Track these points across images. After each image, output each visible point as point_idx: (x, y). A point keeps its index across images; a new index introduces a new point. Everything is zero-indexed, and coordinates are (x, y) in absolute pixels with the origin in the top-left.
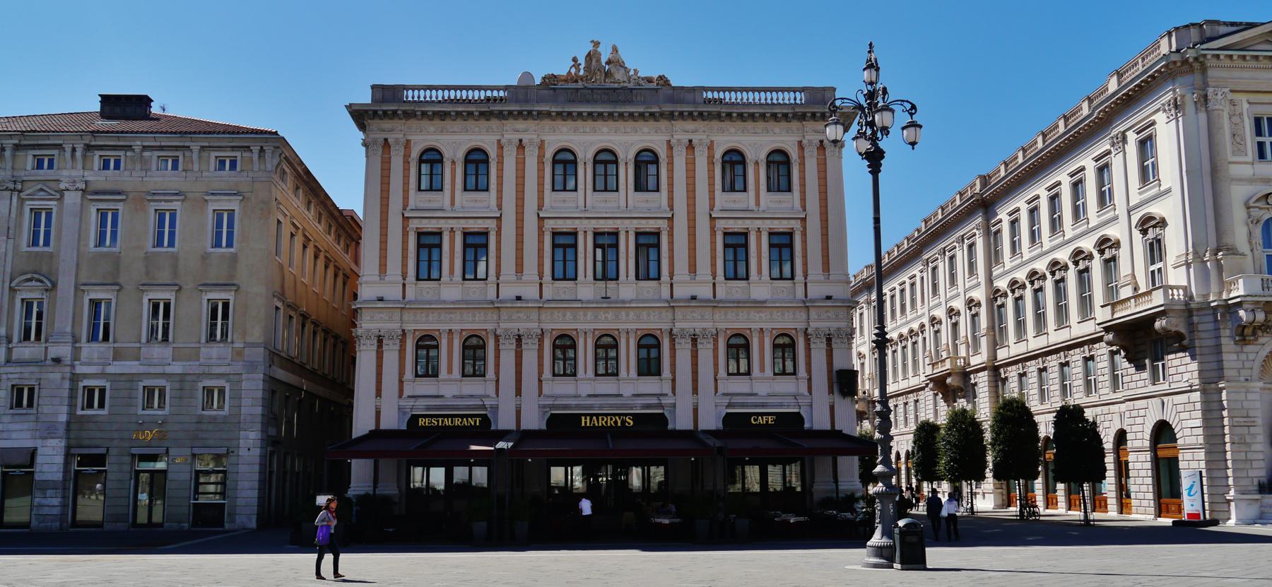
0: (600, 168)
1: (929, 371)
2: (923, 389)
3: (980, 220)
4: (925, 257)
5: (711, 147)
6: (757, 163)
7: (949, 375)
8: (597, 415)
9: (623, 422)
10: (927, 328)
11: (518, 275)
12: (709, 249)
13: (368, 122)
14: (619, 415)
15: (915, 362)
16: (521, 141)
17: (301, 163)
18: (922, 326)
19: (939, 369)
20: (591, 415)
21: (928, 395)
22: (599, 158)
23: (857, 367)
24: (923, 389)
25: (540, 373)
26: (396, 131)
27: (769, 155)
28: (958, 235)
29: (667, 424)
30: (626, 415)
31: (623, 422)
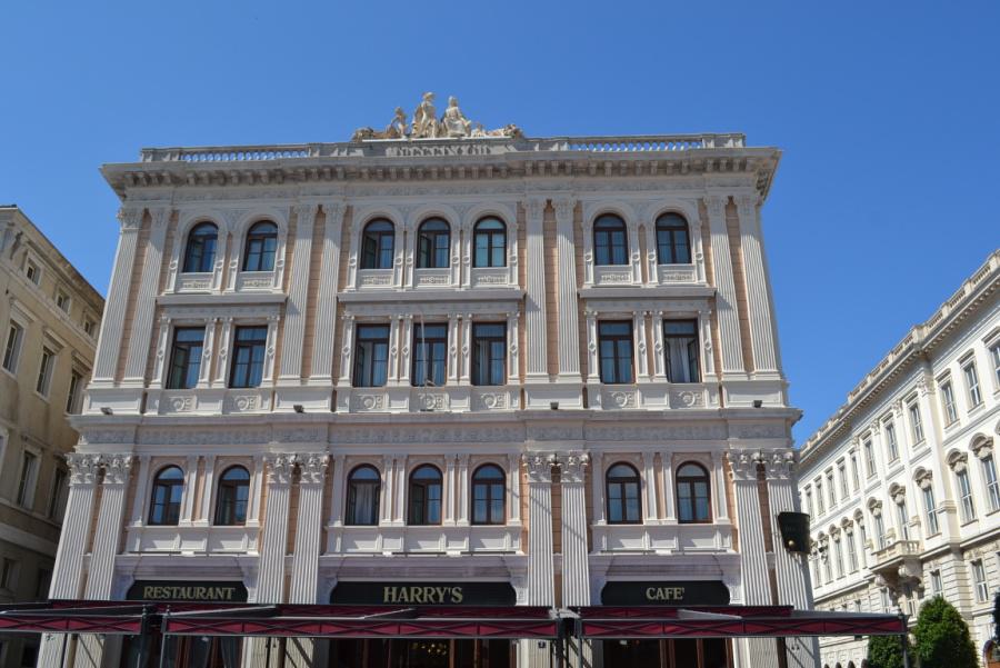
0: (615, 488)
1: (873, 561)
2: (865, 586)
3: (923, 374)
4: (856, 433)
5: (577, 209)
6: (641, 228)
7: (901, 563)
8: (408, 585)
9: (448, 596)
10: (865, 515)
11: (301, 383)
12: (331, 340)
13: (130, 190)
14: (442, 585)
15: (853, 557)
16: (320, 207)
17: (63, 260)
18: (859, 514)
19: (888, 556)
20: (399, 585)
21: (875, 590)
22: (600, 224)
23: (805, 510)
24: (865, 586)
25: (326, 520)
26: (159, 200)
27: (658, 220)
28: (894, 400)
29: (515, 601)
30: (452, 585)
31: (448, 596)
